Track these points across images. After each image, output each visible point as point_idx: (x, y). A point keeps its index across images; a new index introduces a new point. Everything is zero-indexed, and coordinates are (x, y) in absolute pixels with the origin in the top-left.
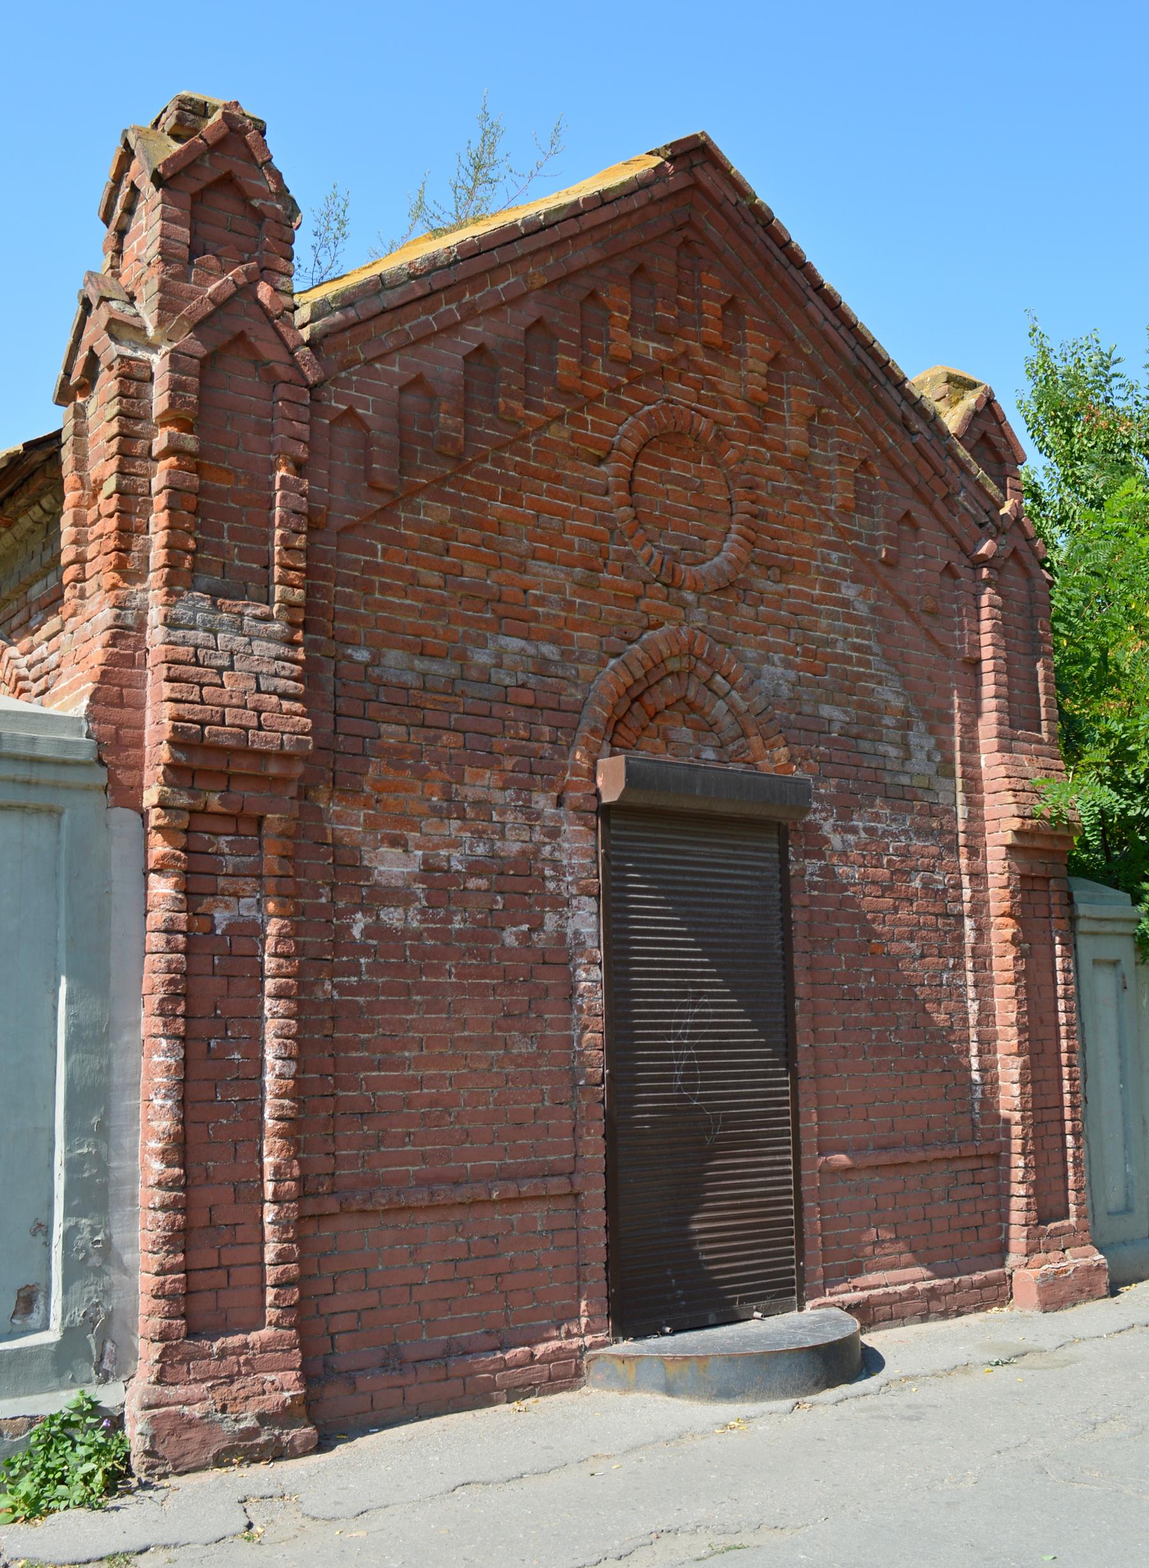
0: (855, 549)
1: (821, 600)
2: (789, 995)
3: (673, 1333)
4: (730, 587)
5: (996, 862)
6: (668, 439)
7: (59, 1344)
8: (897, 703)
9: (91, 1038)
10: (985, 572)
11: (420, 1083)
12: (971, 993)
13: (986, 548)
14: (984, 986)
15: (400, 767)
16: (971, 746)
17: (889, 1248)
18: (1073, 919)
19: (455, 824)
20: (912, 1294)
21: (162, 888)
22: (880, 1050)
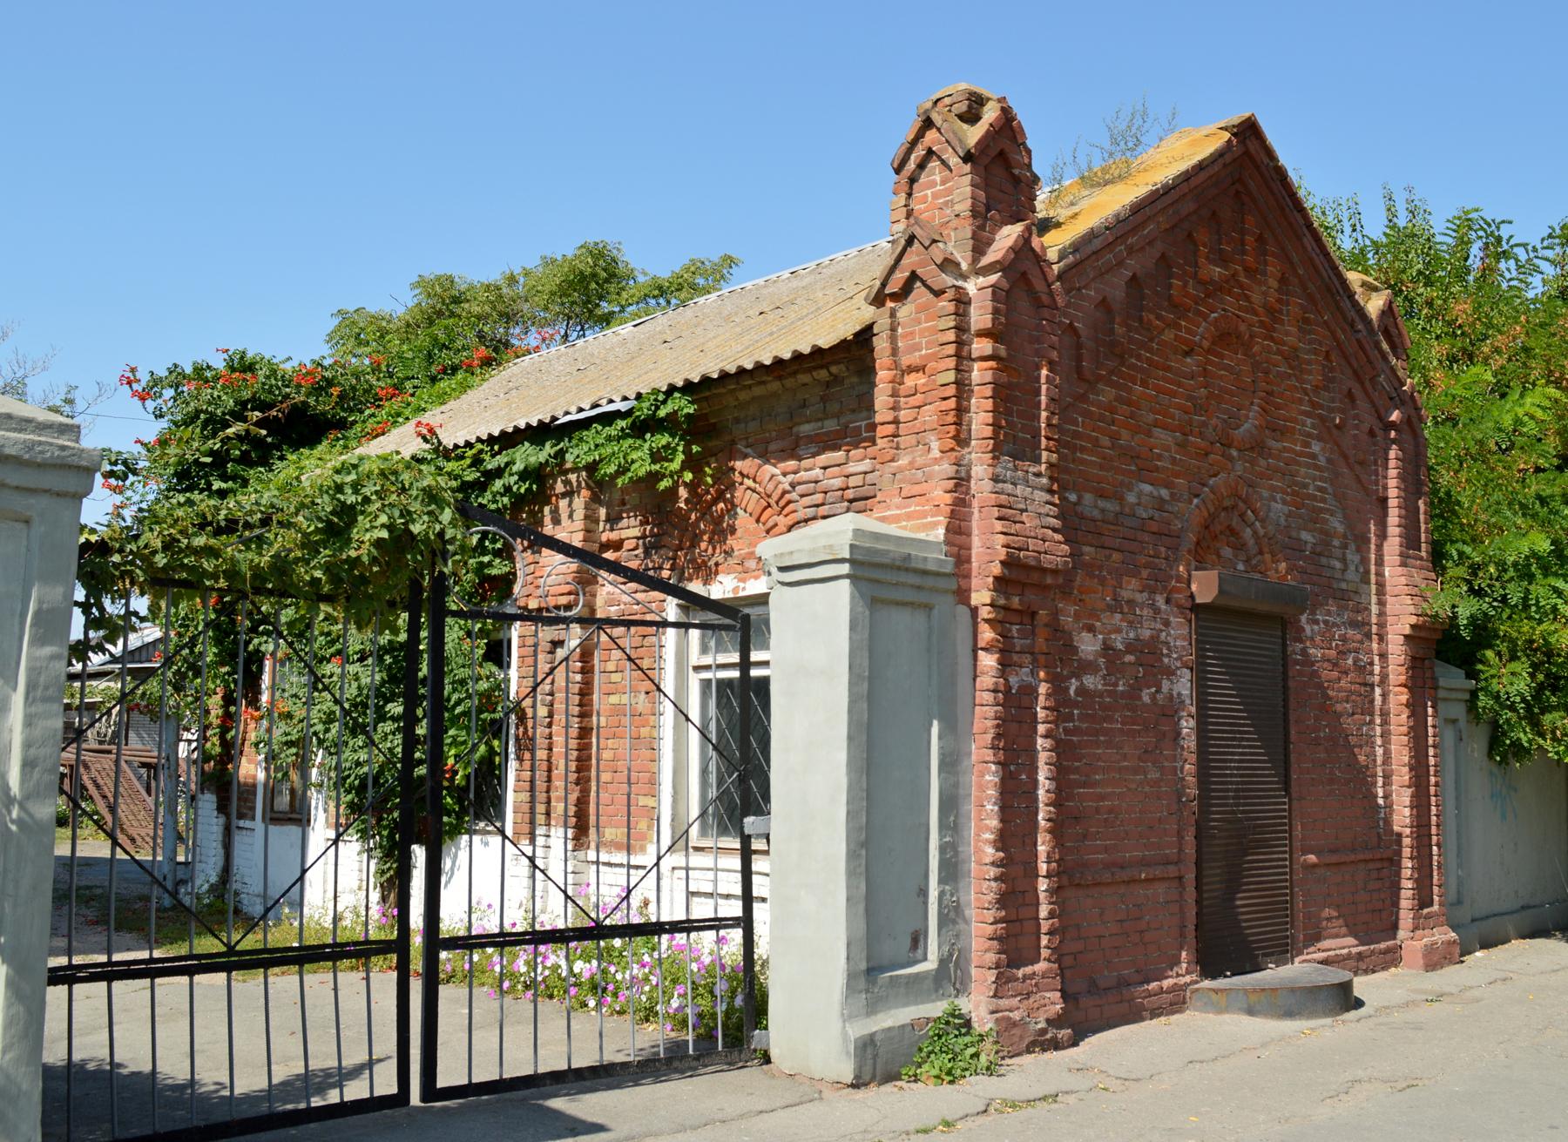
0: (1320, 417)
1: (1301, 454)
2: (1287, 741)
3: (1233, 975)
4: (1256, 447)
5: (1397, 650)
6: (1225, 338)
7: (937, 970)
8: (1340, 529)
9: (950, 763)
10: (1393, 434)
11: (1102, 798)
12: (1379, 741)
13: (1395, 416)
14: (1385, 735)
15: (1092, 576)
16: (1380, 562)
17: (1336, 923)
18: (1436, 688)
19: (1118, 616)
20: (1349, 956)
21: (988, 661)
22: (1331, 781)
